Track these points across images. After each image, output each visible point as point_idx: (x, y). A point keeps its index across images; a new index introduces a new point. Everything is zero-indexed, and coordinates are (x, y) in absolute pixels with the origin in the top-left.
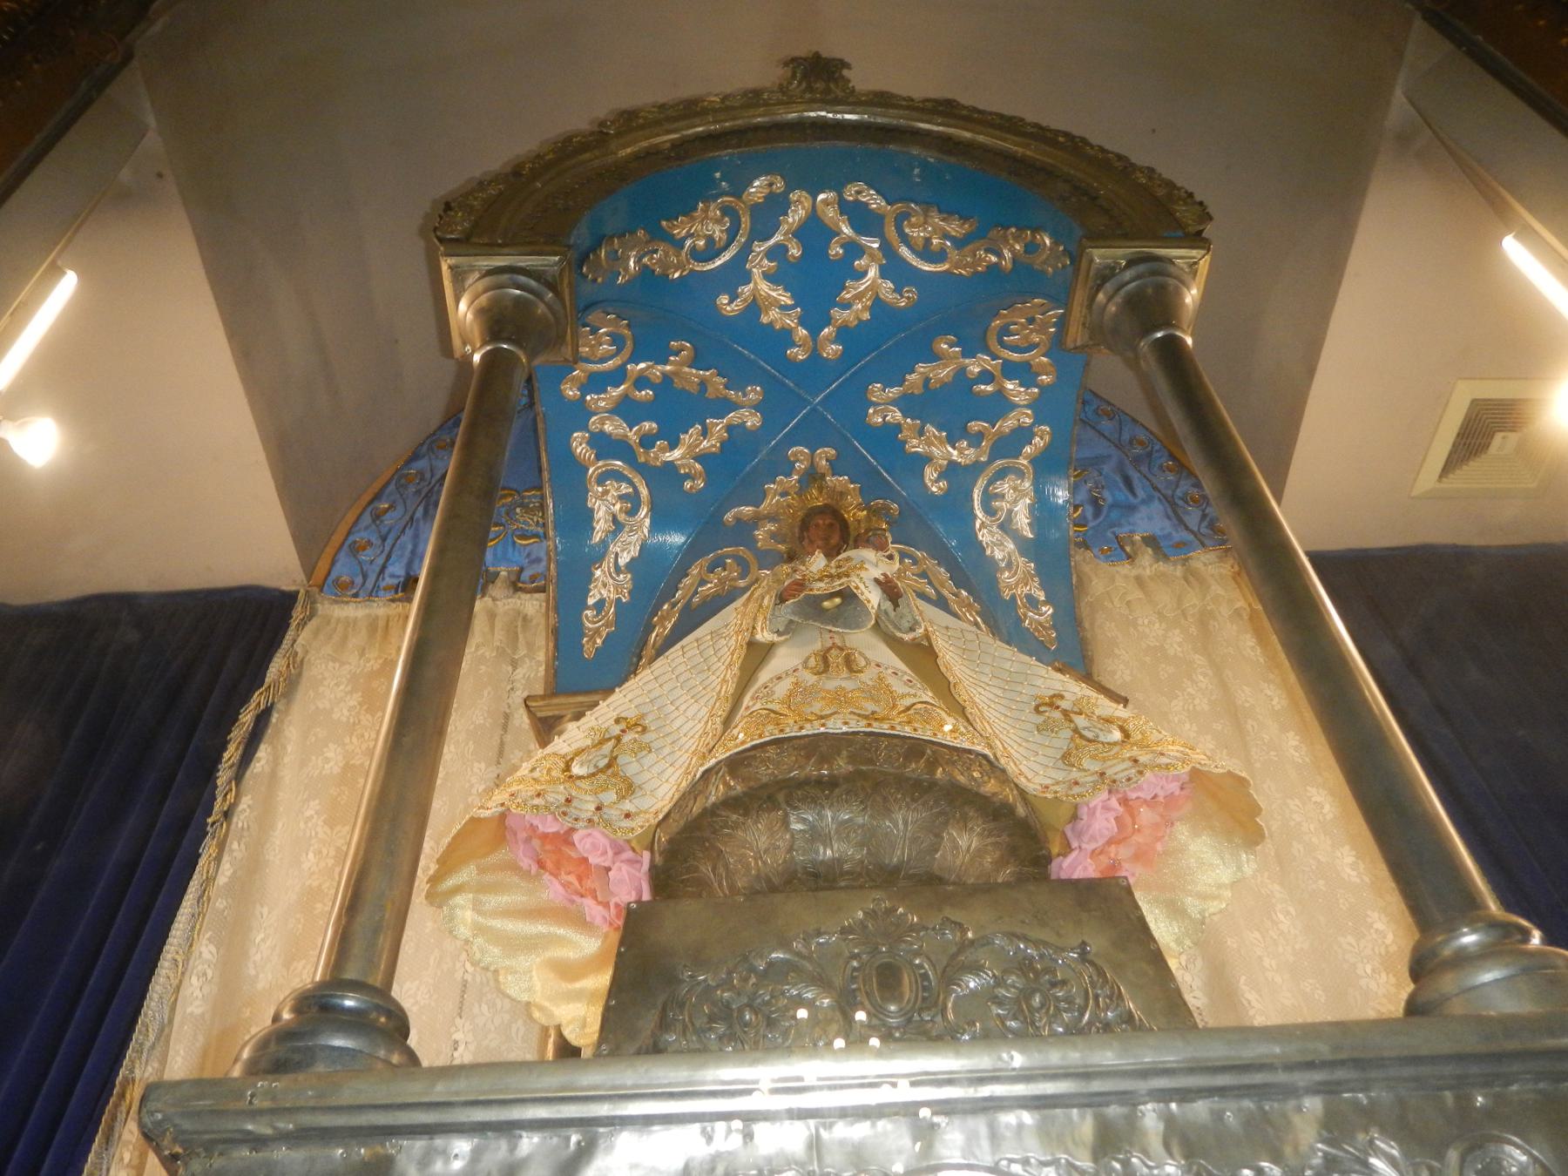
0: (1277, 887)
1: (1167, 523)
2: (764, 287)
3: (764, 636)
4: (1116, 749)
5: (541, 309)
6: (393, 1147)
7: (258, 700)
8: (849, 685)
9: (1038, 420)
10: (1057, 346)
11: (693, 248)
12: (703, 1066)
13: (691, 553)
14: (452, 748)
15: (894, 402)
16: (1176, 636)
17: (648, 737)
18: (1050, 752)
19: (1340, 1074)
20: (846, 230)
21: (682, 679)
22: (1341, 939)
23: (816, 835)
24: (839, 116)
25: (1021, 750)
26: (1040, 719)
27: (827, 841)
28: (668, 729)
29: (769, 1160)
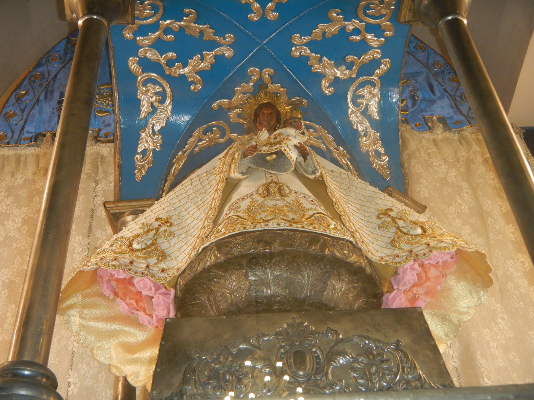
0: (499, 305)
1: (451, 110)
3: (235, 175)
4: (418, 238)
8: (280, 203)
9: (384, 56)
10: (395, 18)
13: (192, 127)
15: (306, 44)
16: (453, 172)
17: (173, 229)
18: (385, 239)
21: (191, 197)
23: (265, 284)
25: (369, 238)
26: (380, 222)
27: (267, 285)
28: (183, 225)
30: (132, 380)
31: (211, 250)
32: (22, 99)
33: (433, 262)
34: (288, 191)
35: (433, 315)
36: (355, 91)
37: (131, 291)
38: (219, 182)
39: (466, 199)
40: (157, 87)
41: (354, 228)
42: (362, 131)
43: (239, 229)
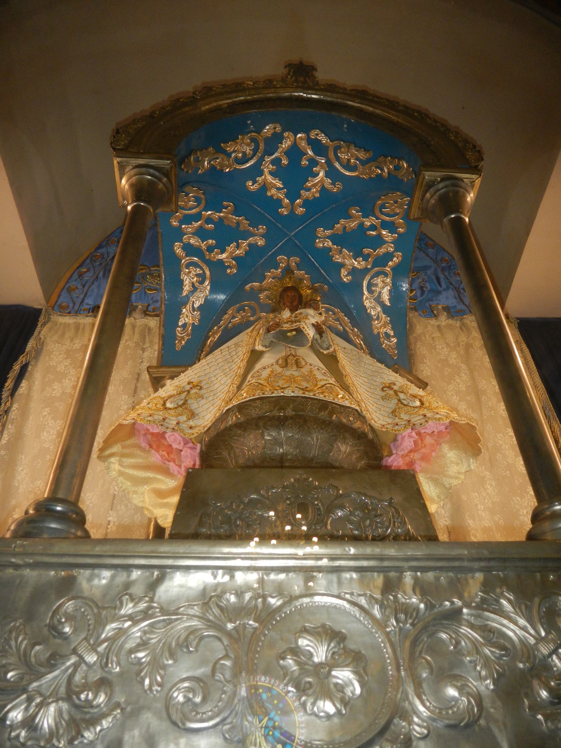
0: (488, 473)
2: (269, 178)
3: (259, 348)
4: (416, 410)
5: (161, 186)
6: (76, 572)
7: (22, 359)
8: (296, 374)
10: (407, 216)
11: (236, 157)
12: (214, 546)
13: (227, 304)
14: (113, 387)
15: (328, 237)
16: (454, 355)
17: (202, 392)
18: (387, 410)
19: (492, 564)
20: (310, 152)
21: (220, 365)
22: (514, 498)
23: (277, 442)
24: (309, 96)
25: (374, 408)
28: (212, 389)
29: (240, 587)
30: (161, 521)
31: (233, 411)
32: (84, 276)
33: (429, 431)
34: (304, 364)
35: (427, 478)
36: (370, 280)
37: (163, 445)
38: (245, 353)
39: (464, 379)
40: (198, 269)
41: (360, 398)
42: (375, 315)
43: (258, 394)
